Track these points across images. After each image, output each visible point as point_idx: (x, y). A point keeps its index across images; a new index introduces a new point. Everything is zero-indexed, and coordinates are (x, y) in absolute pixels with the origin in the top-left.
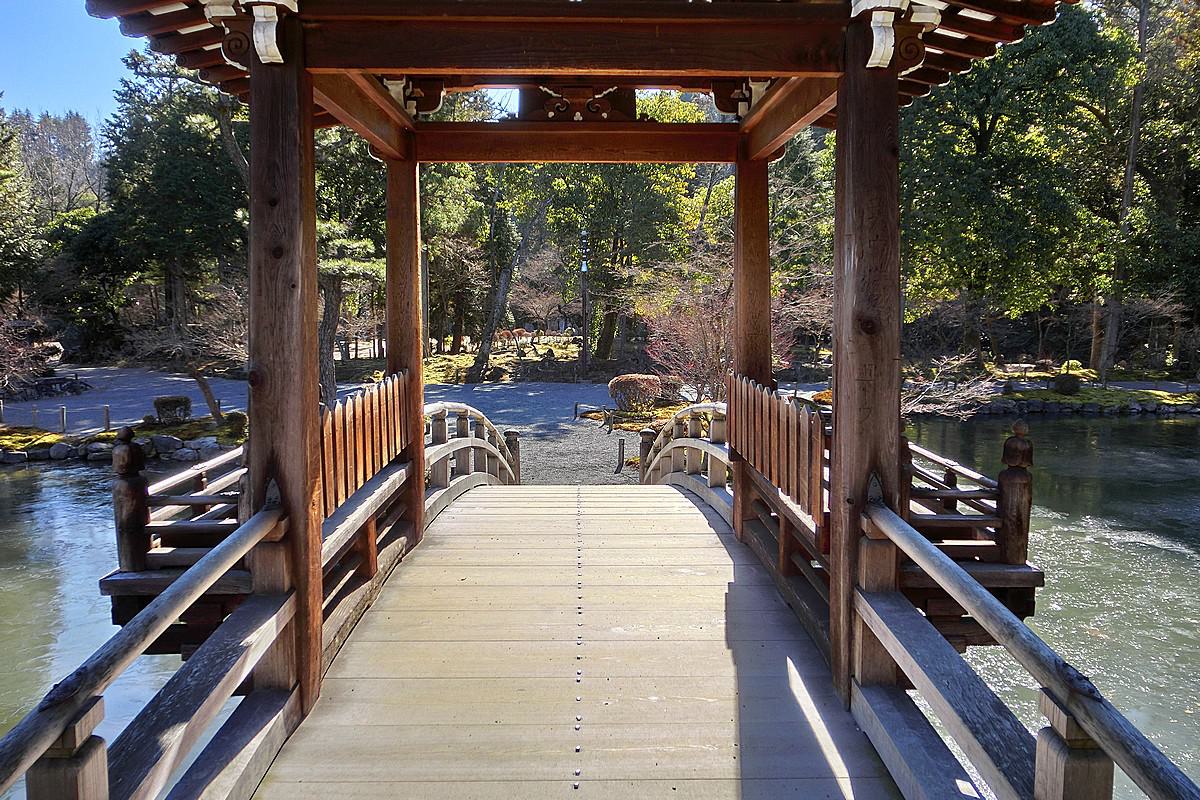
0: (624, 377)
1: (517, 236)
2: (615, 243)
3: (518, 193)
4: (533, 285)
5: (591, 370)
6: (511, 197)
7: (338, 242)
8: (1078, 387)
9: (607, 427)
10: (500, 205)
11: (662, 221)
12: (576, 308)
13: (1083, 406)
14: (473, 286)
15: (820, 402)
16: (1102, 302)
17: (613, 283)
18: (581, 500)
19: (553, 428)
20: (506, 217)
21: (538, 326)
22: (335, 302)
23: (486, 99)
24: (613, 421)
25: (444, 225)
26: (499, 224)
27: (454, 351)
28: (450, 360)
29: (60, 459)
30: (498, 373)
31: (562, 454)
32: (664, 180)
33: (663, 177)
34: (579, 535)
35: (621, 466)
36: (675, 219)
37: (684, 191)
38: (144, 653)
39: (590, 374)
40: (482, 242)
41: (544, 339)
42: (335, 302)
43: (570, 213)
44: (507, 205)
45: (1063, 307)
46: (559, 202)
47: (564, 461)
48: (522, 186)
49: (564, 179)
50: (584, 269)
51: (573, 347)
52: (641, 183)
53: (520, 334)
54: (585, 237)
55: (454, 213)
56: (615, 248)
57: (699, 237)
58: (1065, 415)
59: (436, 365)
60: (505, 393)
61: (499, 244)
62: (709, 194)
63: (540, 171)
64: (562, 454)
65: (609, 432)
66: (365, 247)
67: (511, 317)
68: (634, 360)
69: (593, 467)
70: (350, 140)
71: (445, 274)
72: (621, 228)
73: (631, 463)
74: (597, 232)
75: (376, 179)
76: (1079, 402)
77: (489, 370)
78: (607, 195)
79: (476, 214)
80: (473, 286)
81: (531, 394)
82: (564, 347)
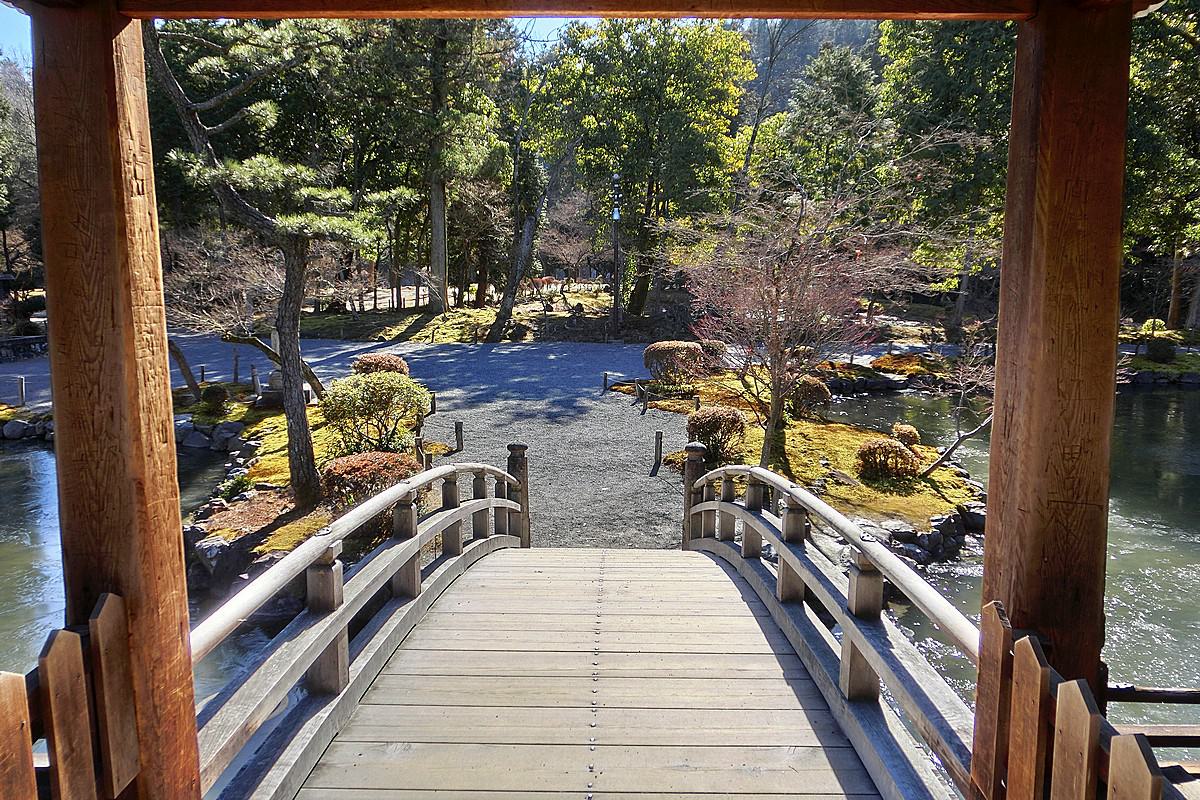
0: (666, 344)
1: (545, 178)
2: (650, 187)
3: (544, 131)
4: (562, 229)
6: (537, 135)
7: (305, 191)
8: (1173, 353)
9: (641, 406)
10: (524, 145)
11: (701, 164)
12: (609, 255)
13: (1181, 376)
14: (497, 234)
15: (879, 369)
16: (1187, 253)
17: (647, 240)
18: (605, 577)
19: (568, 404)
20: (533, 158)
21: (570, 274)
22: (297, 269)
23: (512, 30)
24: (646, 397)
25: (462, 167)
26: (525, 166)
27: (478, 304)
28: (469, 316)
29: (14, 439)
30: (519, 332)
31: (587, 445)
32: (704, 117)
33: (704, 114)
34: (594, 707)
35: (657, 465)
36: (717, 162)
37: (725, 130)
38: (34, 742)
40: (507, 185)
41: (575, 287)
42: (297, 269)
43: (599, 156)
44: (531, 145)
45: (1149, 258)
46: (589, 142)
47: (587, 456)
48: (549, 124)
49: (595, 116)
50: (616, 217)
52: (679, 121)
53: (549, 282)
54: (617, 181)
55: (474, 154)
56: (649, 193)
57: (738, 179)
58: (1160, 386)
59: (454, 321)
60: (526, 357)
61: (526, 187)
62: (755, 132)
63: (568, 108)
64: (587, 445)
66: (339, 198)
67: (538, 265)
69: (624, 466)
70: (307, 58)
71: (467, 219)
72: (657, 171)
73: (671, 462)
74: (630, 173)
75: (388, 116)
76: (1176, 372)
77: (512, 328)
78: (640, 134)
79: (497, 155)
80: (497, 234)
81: (552, 357)
82: (589, 297)
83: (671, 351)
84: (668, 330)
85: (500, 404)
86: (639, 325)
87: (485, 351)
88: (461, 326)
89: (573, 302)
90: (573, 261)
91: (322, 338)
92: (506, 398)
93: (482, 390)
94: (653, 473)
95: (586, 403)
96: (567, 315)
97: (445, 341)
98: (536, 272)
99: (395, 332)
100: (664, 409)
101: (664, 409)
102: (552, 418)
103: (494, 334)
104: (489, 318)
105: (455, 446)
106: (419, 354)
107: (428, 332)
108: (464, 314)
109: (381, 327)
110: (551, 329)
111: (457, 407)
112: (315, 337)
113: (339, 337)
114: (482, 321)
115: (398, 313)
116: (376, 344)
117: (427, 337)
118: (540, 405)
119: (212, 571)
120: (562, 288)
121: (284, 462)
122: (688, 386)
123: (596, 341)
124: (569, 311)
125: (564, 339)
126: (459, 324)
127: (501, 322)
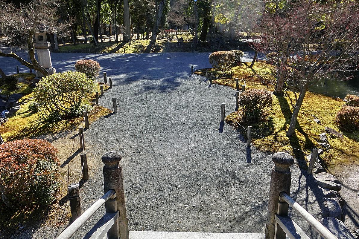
0: (216, 53)
4: (176, 13)
5: (198, 46)
9: (208, 82)
19: (171, 81)
21: (179, 28)
24: (209, 76)
30: (158, 48)
31: (183, 108)
39: (198, 48)
41: (180, 33)
47: (184, 116)
51: (191, 36)
60: (158, 59)
64: (183, 108)
65: (210, 86)
67: (167, 24)
68: (217, 42)
82: (187, 36)
83: (220, 56)
84: (216, 46)
85: (139, 82)
86: (205, 45)
87: (143, 56)
88: (136, 47)
89: (179, 37)
90: (180, 24)
91: (82, 52)
92: (144, 78)
93: (136, 74)
94: (221, 131)
95: (179, 80)
96: (177, 41)
97: (129, 52)
98: (166, 27)
99: (110, 49)
100: (220, 84)
101: (220, 84)
102: (163, 89)
103: (148, 50)
104: (147, 43)
105: (112, 109)
106: (116, 58)
107: (122, 49)
108: (137, 42)
109: (104, 48)
110: (169, 47)
111: (120, 83)
112: (80, 52)
113: (89, 52)
114: (144, 45)
115: (110, 44)
116: (102, 54)
117: (122, 51)
118: (158, 82)
119: (308, 163)
120: (176, 33)
121: (279, 106)
122: (229, 71)
123: (188, 51)
124: (178, 40)
125: (175, 51)
126: (135, 46)
127: (151, 44)
